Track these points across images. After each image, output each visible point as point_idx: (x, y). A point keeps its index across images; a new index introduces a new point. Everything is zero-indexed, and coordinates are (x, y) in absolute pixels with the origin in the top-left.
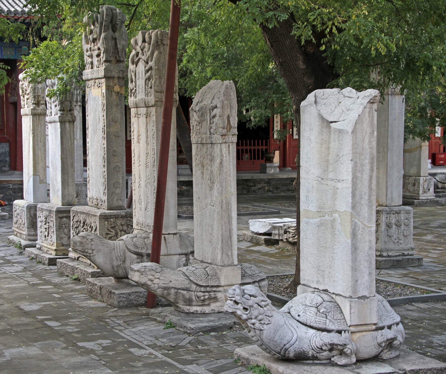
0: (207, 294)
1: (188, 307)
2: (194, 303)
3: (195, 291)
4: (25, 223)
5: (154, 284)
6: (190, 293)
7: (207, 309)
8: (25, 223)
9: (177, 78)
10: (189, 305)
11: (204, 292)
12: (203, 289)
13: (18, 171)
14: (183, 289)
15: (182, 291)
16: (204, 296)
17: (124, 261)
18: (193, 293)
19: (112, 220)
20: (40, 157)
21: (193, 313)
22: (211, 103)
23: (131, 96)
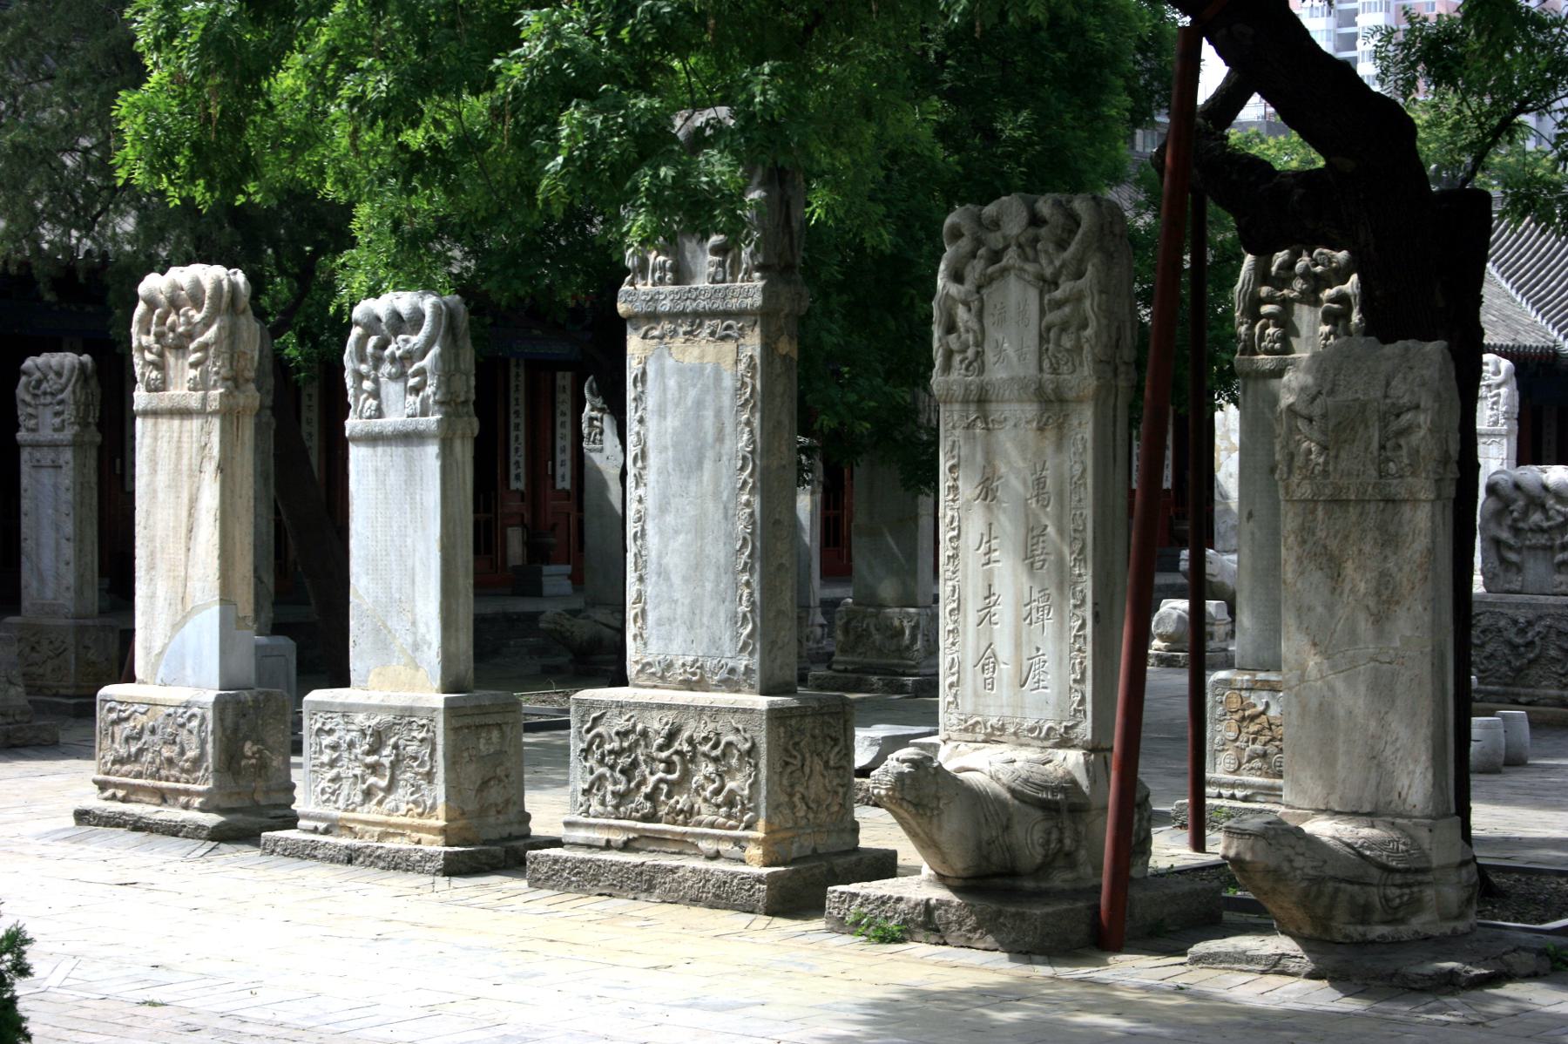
0: (1407, 891)
1: (1360, 928)
2: (1376, 917)
3: (1378, 886)
4: (202, 755)
5: (1295, 869)
6: (1368, 889)
7: (1404, 931)
8: (202, 755)
9: (936, 335)
10: (1363, 922)
11: (1400, 886)
12: (1398, 879)
13: (556, 562)
14: (1351, 882)
15: (1349, 888)
16: (1401, 896)
17: (1007, 828)
18: (1375, 890)
19: (793, 722)
20: (238, 546)
21: (1373, 942)
22: (1386, 396)
23: (947, 367)
